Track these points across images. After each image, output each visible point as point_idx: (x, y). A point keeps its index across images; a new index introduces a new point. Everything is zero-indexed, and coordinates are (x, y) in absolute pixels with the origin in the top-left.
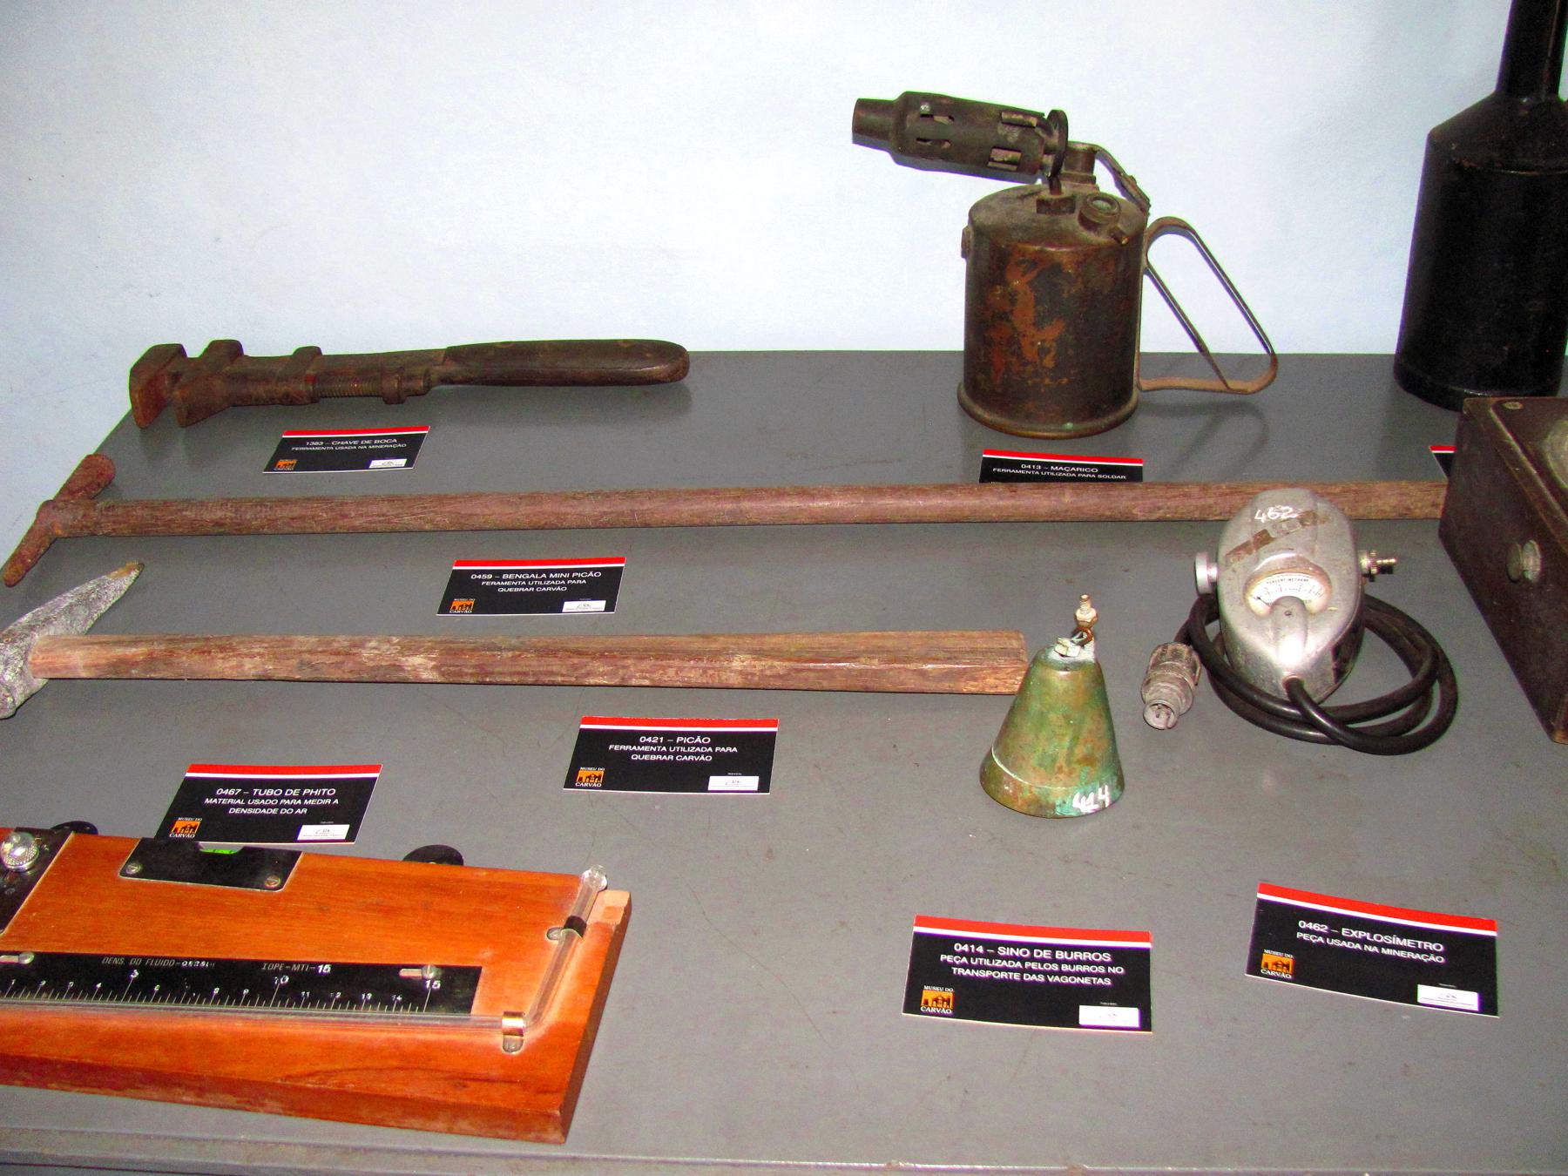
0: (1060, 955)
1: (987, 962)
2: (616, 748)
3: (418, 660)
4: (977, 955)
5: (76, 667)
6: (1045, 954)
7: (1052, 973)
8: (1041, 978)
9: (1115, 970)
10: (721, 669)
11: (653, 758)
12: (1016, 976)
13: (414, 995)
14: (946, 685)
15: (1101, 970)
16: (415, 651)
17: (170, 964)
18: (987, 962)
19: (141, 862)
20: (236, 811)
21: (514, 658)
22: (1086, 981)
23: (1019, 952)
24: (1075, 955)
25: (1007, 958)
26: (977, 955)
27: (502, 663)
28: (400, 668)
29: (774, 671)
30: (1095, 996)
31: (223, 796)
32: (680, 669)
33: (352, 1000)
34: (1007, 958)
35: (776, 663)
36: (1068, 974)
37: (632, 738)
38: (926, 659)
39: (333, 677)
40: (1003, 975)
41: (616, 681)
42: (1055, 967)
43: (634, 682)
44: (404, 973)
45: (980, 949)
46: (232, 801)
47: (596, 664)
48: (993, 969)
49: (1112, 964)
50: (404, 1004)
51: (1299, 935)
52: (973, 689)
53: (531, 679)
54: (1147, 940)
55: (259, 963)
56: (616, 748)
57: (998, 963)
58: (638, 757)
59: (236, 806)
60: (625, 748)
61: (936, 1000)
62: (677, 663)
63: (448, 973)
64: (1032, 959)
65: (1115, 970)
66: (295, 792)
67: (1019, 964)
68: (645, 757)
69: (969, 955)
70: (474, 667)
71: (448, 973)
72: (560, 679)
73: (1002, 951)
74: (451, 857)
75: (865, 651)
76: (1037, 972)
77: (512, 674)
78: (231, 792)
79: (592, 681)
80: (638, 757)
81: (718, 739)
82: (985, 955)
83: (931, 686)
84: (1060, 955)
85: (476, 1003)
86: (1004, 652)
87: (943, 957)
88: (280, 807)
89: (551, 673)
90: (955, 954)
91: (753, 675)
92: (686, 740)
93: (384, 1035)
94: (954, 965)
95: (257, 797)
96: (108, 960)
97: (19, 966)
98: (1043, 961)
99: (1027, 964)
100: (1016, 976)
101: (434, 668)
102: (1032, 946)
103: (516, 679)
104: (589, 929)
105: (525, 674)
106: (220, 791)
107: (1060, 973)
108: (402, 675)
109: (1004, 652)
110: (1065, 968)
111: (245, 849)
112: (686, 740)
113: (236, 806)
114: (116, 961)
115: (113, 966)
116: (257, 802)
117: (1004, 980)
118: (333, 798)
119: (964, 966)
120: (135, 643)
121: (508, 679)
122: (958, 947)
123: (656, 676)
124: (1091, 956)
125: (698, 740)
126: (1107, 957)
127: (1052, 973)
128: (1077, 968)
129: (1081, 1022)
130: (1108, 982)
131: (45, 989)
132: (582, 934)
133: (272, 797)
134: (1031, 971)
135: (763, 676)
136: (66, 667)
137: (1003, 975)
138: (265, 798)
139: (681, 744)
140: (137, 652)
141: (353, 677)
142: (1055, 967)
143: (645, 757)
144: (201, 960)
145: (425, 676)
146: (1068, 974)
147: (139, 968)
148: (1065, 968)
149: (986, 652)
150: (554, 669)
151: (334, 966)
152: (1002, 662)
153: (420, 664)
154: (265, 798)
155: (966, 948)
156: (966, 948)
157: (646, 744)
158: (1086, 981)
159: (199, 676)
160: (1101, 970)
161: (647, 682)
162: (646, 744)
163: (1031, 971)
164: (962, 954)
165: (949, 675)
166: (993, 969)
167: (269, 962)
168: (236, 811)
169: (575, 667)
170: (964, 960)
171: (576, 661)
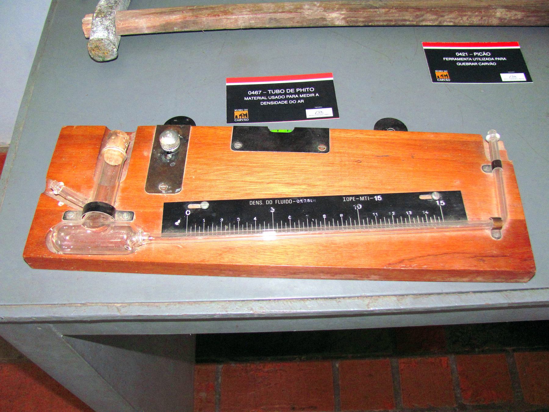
2: (447, 59)
3: (334, 15)
5: (142, 28)
10: (489, 17)
11: (468, 64)
13: (432, 210)
16: (333, 10)
17: (290, 202)
19: (241, 141)
20: (265, 103)
21: (386, 13)
27: (380, 16)
28: (324, 19)
29: (516, 17)
31: (252, 95)
32: (470, 17)
33: (401, 216)
37: (452, 53)
39: (288, 25)
41: (436, 23)
43: (445, 24)
44: (422, 197)
46: (259, 98)
47: (428, 15)
50: (430, 215)
53: (393, 23)
55: (341, 197)
56: (447, 59)
58: (460, 64)
59: (263, 101)
60: (452, 59)
61: (241, 115)
62: (469, 13)
63: (445, 195)
66: (292, 91)
68: (464, 64)
70: (364, 17)
71: (445, 195)
72: (408, 23)
74: (400, 126)
77: (384, 21)
78: (256, 93)
79: (424, 23)
80: (460, 64)
81: (495, 53)
85: (467, 212)
88: (288, 99)
89: (405, 20)
91: (505, 19)
92: (479, 54)
93: (429, 235)
95: (272, 95)
96: (253, 203)
97: (201, 209)
101: (344, 18)
103: (385, 24)
104: (502, 163)
105: (391, 21)
106: (250, 93)
108: (325, 23)
111: (297, 130)
112: (479, 54)
113: (263, 101)
114: (258, 203)
115: (257, 206)
116: (273, 97)
118: (315, 93)
120: (172, 12)
121: (381, 24)
123: (457, 21)
125: (484, 54)
129: (308, 117)
131: (224, 223)
132: (501, 167)
133: (281, 94)
135: (510, 20)
136: (136, 29)
138: (275, 95)
139: (477, 56)
140: (175, 18)
141: (527, 24)
143: (464, 64)
144: (307, 198)
145: (337, 23)
147: (274, 205)
150: (407, 18)
151: (382, 195)
153: (336, 17)
154: (275, 95)
157: (460, 57)
159: (212, 29)
161: (451, 24)
162: (460, 57)
167: (346, 196)
168: (265, 103)
169: (417, 17)
171: (418, 13)
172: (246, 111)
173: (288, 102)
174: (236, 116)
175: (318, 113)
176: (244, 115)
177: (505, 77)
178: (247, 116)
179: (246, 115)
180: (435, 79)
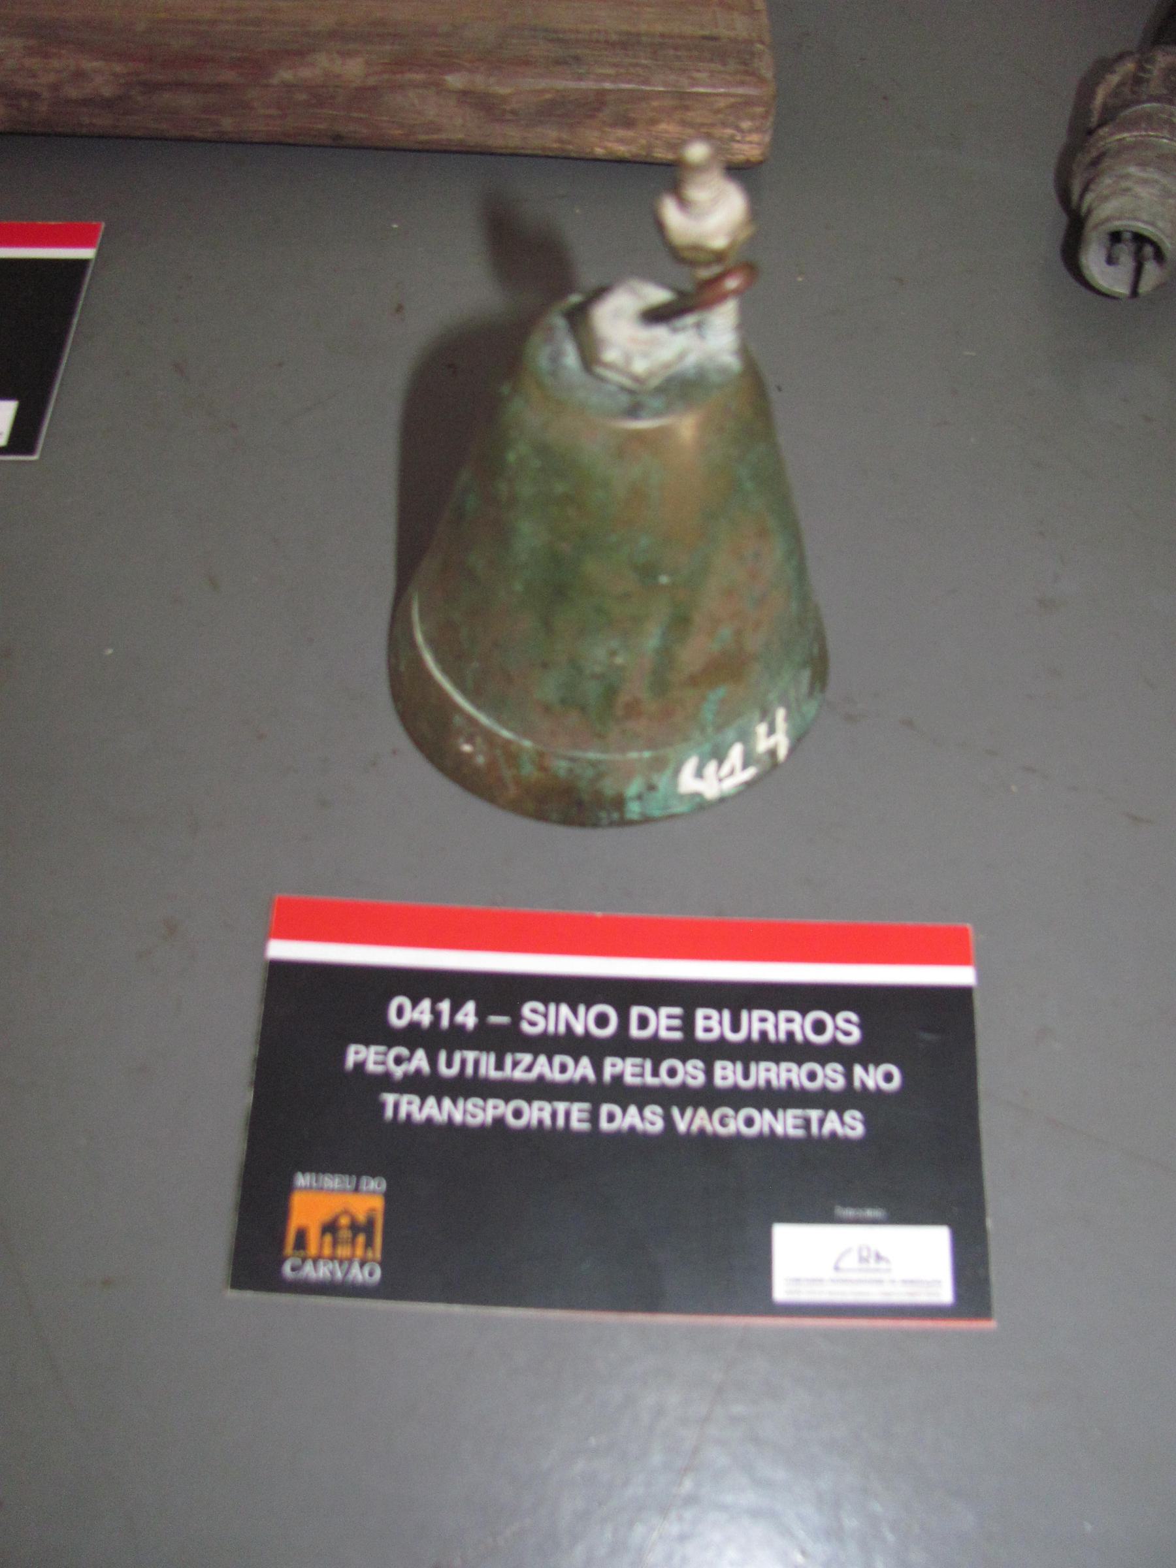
0: (711, 1024)
1: (487, 1066)
4: (457, 1038)
6: (663, 1022)
7: (685, 1097)
8: (650, 1120)
9: (871, 1077)
12: (577, 1115)
14: (549, 137)
15: (831, 1076)
18: (487, 1066)
22: (786, 1123)
23: (583, 1021)
24: (758, 1023)
25: (547, 1045)
26: (457, 1038)
30: (824, 1184)
34: (547, 1045)
35: (90, 64)
36: (736, 1098)
38: (494, 59)
40: (537, 1113)
42: (691, 1073)
45: (468, 1016)
48: (507, 1090)
49: (865, 1054)
52: (622, 150)
54: (961, 959)
57: (523, 1067)
61: (330, 1228)
64: (622, 1045)
65: (871, 1077)
67: (584, 1069)
69: (431, 1039)
73: (537, 1018)
75: (333, 35)
76: (641, 1096)
82: (482, 1039)
83: (511, 136)
84: (711, 1024)
86: (712, 49)
87: (355, 1054)
90: (390, 1037)
91: (34, 96)
94: (386, 1082)
98: (655, 1050)
99: (612, 1066)
100: (577, 1115)
102: (624, 993)
107: (709, 1097)
109: (712, 49)
110: (727, 1074)
117: (537, 1135)
119: (420, 1085)
122: (406, 1012)
124: (793, 1024)
126: (846, 1027)
127: (685, 1097)
128: (766, 1073)
129: (782, 1292)
130: (852, 1125)
134: (622, 1094)
137: (537, 1113)
142: (691, 1073)
146: (736, 1098)
148: (727, 1074)
149: (663, 48)
152: (704, 83)
155: (423, 1014)
156: (423, 1014)
158: (786, 1123)
160: (831, 1076)
163: (622, 1094)
164: (413, 1037)
165: (556, 109)
166: (507, 1090)
170: (420, 1061)
172: (368, 1199)
173: (849, 1076)
174: (301, 1236)
175: (851, 1261)
176: (355, 1228)
177: (811, 1259)
178: (369, 1244)
179: (368, 1228)
180: (258, 1251)
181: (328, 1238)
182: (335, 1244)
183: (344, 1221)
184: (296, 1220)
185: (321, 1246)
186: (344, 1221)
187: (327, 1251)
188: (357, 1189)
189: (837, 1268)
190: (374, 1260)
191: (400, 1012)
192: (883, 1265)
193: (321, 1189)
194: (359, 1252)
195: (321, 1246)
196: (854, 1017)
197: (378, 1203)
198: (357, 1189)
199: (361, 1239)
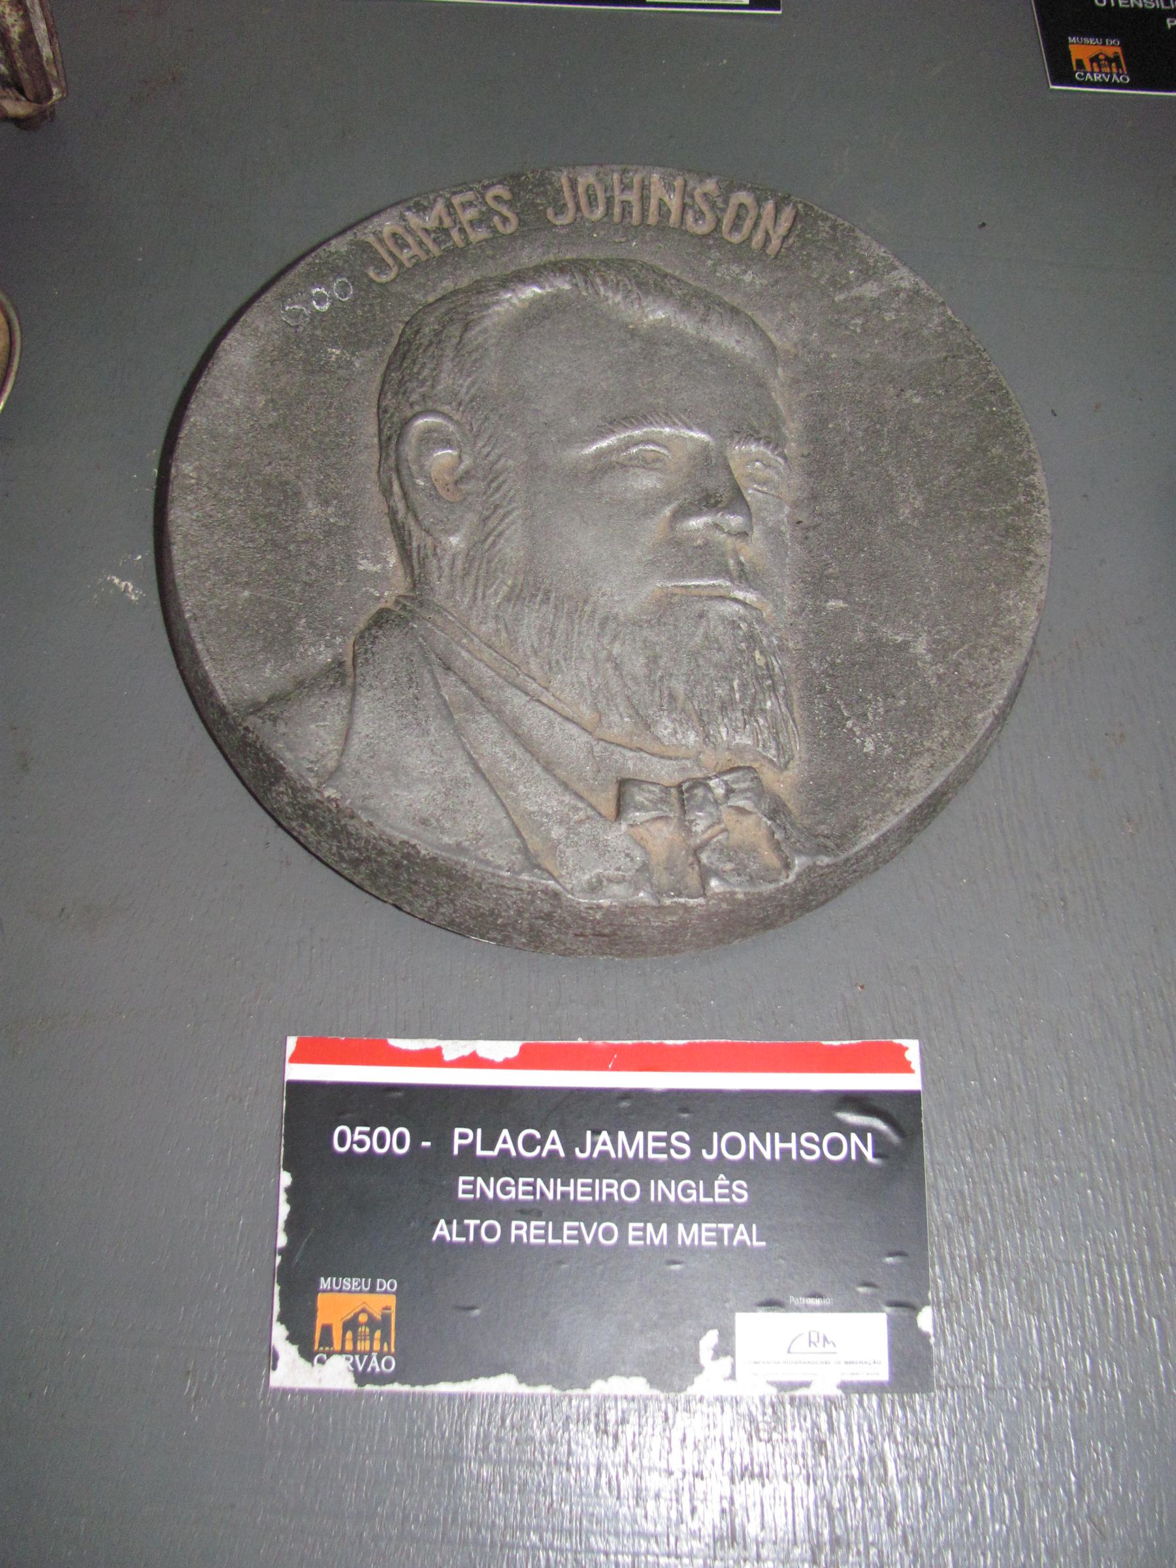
51: (652, 1182)
61: (351, 1325)
174: (327, 1330)
176: (372, 1323)
178: (385, 1338)
179: (1116, 59)
181: (1095, 65)
182: (1100, 66)
183: (363, 1318)
184: (1074, 57)
185: (343, 1342)
186: (363, 1318)
187: (349, 1346)
188: (373, 1290)
189: (789, 1352)
190: (389, 1353)
191: (342, 1140)
192: (829, 1347)
193: (340, 1291)
194: (377, 1346)
195: (343, 1342)
196: (745, 1184)
197: (391, 1301)
198: (1104, 44)
199: (378, 1334)
